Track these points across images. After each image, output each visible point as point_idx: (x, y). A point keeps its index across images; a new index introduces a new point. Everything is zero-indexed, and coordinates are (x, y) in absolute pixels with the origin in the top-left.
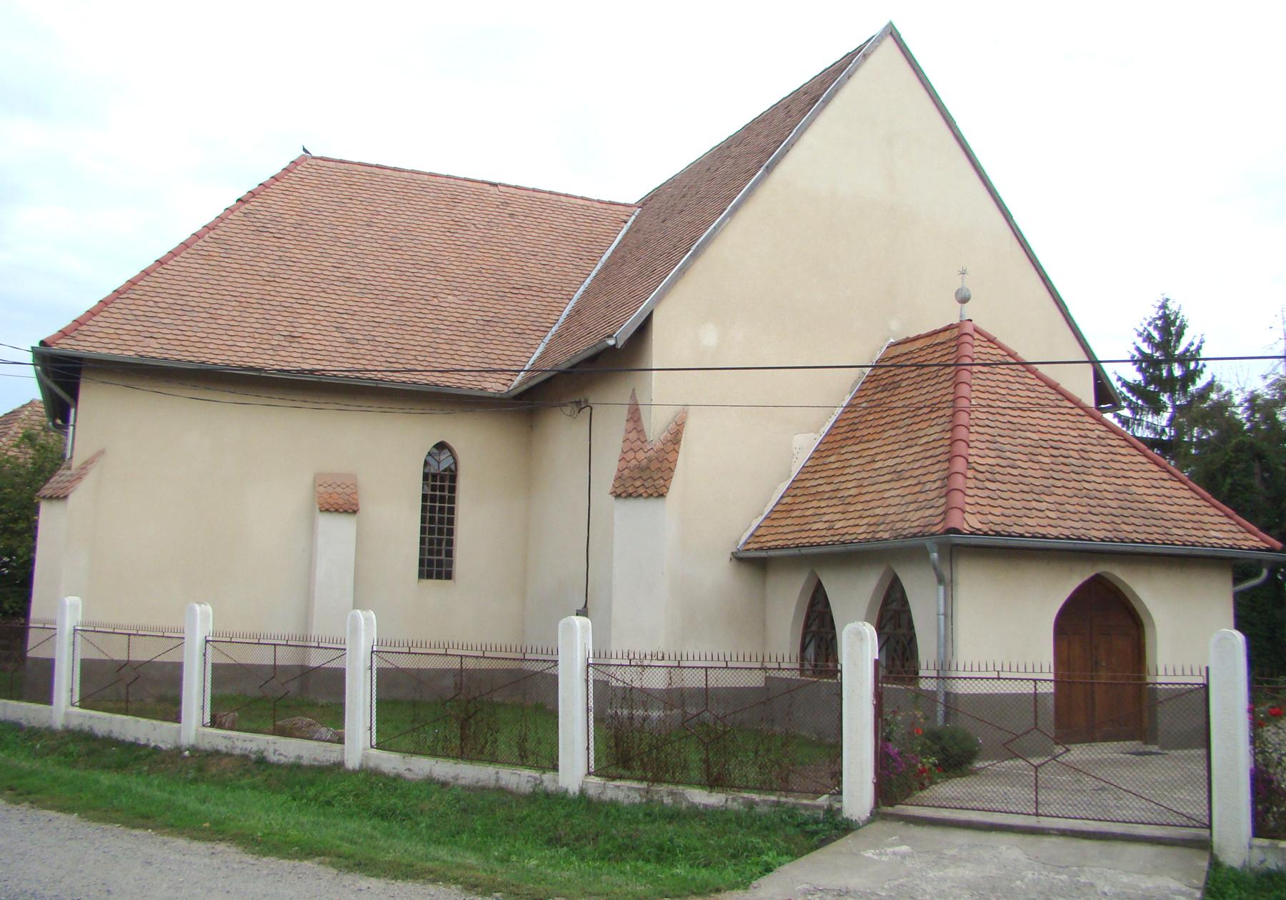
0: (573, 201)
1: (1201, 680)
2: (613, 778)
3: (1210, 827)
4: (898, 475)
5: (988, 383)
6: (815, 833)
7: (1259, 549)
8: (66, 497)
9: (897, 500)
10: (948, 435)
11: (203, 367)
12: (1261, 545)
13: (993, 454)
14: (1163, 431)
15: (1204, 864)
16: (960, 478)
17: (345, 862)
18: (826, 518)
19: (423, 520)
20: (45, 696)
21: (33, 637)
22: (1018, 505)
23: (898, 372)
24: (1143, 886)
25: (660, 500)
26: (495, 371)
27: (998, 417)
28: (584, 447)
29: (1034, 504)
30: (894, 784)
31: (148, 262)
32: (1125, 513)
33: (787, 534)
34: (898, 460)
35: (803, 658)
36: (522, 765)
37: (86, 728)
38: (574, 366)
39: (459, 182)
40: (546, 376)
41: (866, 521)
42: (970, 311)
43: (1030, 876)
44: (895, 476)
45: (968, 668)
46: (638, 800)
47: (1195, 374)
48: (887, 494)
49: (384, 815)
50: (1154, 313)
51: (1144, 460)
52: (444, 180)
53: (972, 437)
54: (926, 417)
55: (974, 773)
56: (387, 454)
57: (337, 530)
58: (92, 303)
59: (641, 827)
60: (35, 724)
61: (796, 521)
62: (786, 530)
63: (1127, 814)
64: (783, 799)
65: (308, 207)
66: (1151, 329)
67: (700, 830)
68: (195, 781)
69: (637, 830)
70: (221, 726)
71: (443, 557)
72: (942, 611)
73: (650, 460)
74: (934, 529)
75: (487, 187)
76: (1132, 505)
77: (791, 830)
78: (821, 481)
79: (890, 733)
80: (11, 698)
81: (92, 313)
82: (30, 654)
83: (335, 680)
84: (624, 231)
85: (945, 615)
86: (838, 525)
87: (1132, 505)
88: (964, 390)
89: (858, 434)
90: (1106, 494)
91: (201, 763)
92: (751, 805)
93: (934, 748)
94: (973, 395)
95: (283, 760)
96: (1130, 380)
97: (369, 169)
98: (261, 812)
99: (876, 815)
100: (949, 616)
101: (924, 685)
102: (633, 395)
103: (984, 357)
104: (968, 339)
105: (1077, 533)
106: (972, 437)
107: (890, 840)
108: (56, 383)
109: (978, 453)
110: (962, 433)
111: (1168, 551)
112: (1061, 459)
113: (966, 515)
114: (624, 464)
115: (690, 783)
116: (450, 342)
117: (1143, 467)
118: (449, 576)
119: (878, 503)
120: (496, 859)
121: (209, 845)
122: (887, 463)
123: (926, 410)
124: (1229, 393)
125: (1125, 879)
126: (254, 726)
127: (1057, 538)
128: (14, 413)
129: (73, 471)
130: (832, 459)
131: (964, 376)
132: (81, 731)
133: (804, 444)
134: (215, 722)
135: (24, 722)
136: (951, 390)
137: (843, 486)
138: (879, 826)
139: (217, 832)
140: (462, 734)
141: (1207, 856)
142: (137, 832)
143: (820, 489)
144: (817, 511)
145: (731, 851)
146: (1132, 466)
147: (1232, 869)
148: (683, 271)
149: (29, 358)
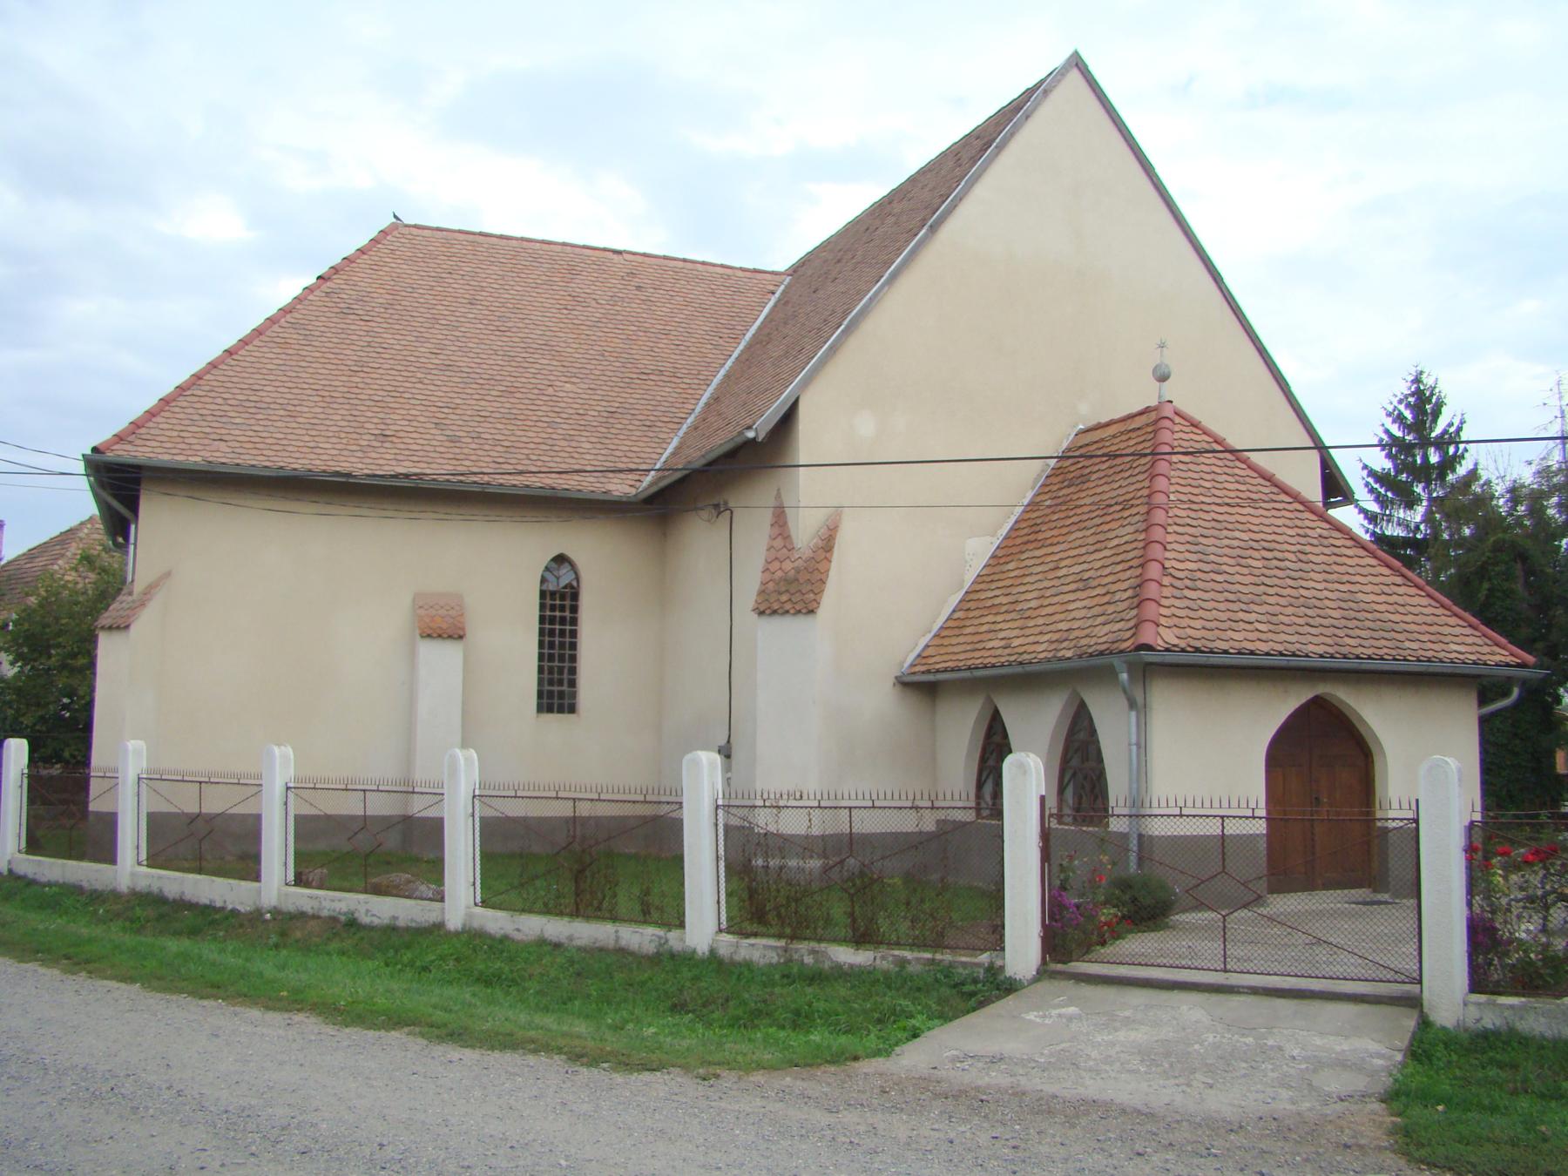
0: (711, 269)
1: (1410, 815)
2: (748, 936)
3: (1420, 982)
4: (1084, 584)
5: (1190, 474)
6: (972, 994)
7: (1508, 665)
8: (127, 627)
9: (1083, 613)
10: (1142, 536)
11: (282, 473)
12: (1509, 659)
13: (1194, 557)
14: (1417, 527)
15: (1410, 1022)
16: (1154, 585)
17: (436, 1032)
18: (1001, 635)
19: (541, 644)
20: (107, 853)
21: (95, 787)
22: (1223, 616)
23: (1086, 463)
24: (1338, 1048)
25: (810, 618)
26: (621, 471)
27: (1201, 515)
28: (723, 557)
29: (1241, 615)
30: (1065, 939)
31: (215, 352)
32: (1350, 624)
33: (959, 655)
34: (1085, 566)
35: (979, 796)
36: (645, 922)
37: (155, 889)
38: (710, 464)
39: (577, 250)
40: (678, 475)
41: (1046, 637)
42: (1170, 390)
43: (1211, 1039)
44: (1081, 585)
45: (1163, 804)
46: (775, 960)
47: (1457, 458)
48: (1072, 606)
49: (487, 981)
50: (1404, 388)
51: (1373, 562)
52: (559, 248)
53: (1170, 538)
54: (1117, 516)
55: (1167, 927)
56: (498, 572)
57: (441, 660)
58: (150, 402)
59: (777, 990)
60: (99, 887)
61: (969, 639)
62: (961, 648)
63: (1338, 970)
64: (938, 956)
65: (404, 281)
66: (1402, 407)
67: (843, 992)
68: (276, 946)
69: (772, 994)
70: (308, 885)
71: (565, 688)
72: (1134, 740)
73: (798, 571)
74: (1124, 646)
75: (610, 255)
76: (1359, 615)
77: (946, 991)
78: (997, 592)
79: (1066, 879)
80: (70, 857)
81: (151, 414)
82: (92, 807)
83: (435, 828)
84: (771, 304)
85: (1139, 746)
86: (1016, 643)
87: (1359, 615)
88: (1161, 483)
89: (1040, 536)
90: (1327, 603)
91: (284, 928)
92: (902, 963)
93: (1117, 900)
94: (1172, 489)
95: (376, 921)
96: (1377, 468)
97: (471, 238)
98: (344, 978)
99: (1043, 973)
100: (1142, 746)
101: (1116, 825)
102: (778, 496)
103: (1185, 444)
104: (1167, 423)
105: (1292, 648)
106: (1170, 538)
107: (1056, 1001)
108: (115, 496)
109: (1178, 557)
110: (1158, 533)
111: (1401, 668)
112: (1275, 563)
113: (1161, 630)
114: (768, 576)
115: (836, 940)
116: (568, 438)
117: (1373, 571)
118: (572, 709)
119: (1062, 616)
120: (609, 1027)
121: (286, 1015)
122: (1072, 570)
123: (1118, 508)
124: (1488, 483)
125: (1318, 1041)
126: (346, 884)
127: (1267, 654)
128: (71, 532)
129: (135, 596)
130: (1011, 566)
131: (1162, 467)
132: (149, 894)
133: (979, 550)
134: (300, 880)
135: (85, 884)
136: (1146, 484)
137: (1023, 597)
138: (1046, 986)
139: (297, 1002)
140: (577, 888)
141: (1415, 1014)
142: (205, 1003)
143: (997, 601)
144: (993, 627)
145: (876, 1015)
146: (1359, 570)
147: (1444, 1028)
148: (833, 350)
149: (80, 467)
